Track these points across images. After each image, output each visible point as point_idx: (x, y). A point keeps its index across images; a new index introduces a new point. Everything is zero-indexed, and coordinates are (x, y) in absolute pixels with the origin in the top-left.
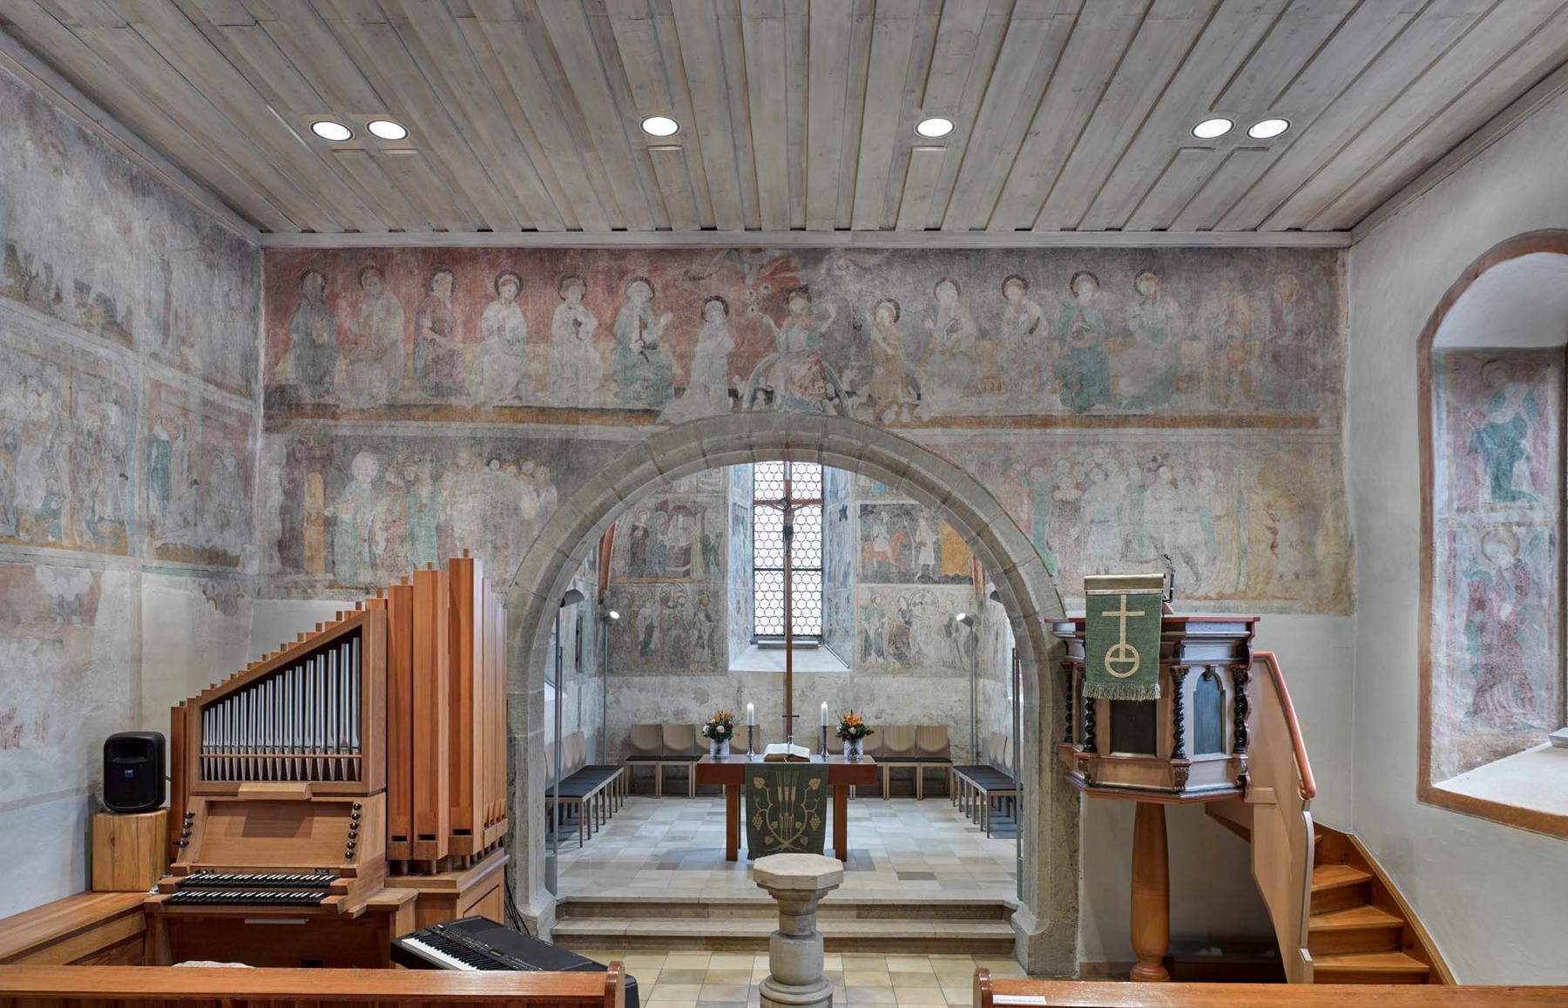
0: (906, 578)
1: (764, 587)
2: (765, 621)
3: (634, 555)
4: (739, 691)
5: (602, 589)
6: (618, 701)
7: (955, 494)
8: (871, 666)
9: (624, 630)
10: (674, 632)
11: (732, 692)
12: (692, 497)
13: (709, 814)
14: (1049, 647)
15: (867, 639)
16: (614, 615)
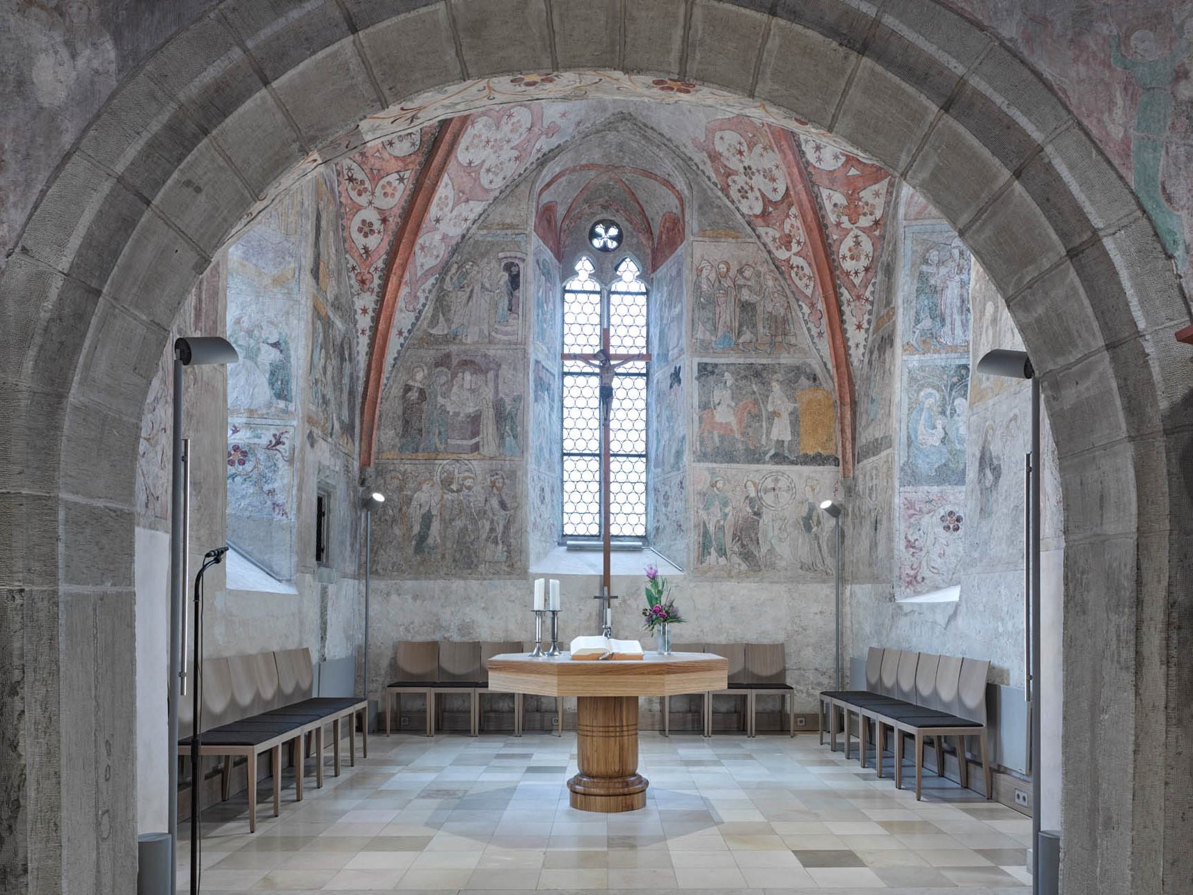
0: (754, 456)
1: (576, 476)
2: (576, 518)
5: (364, 466)
7: (975, 82)
8: (710, 568)
9: (394, 520)
10: (458, 524)
13: (498, 756)
14: (1164, 405)
15: (706, 533)
16: (378, 497)
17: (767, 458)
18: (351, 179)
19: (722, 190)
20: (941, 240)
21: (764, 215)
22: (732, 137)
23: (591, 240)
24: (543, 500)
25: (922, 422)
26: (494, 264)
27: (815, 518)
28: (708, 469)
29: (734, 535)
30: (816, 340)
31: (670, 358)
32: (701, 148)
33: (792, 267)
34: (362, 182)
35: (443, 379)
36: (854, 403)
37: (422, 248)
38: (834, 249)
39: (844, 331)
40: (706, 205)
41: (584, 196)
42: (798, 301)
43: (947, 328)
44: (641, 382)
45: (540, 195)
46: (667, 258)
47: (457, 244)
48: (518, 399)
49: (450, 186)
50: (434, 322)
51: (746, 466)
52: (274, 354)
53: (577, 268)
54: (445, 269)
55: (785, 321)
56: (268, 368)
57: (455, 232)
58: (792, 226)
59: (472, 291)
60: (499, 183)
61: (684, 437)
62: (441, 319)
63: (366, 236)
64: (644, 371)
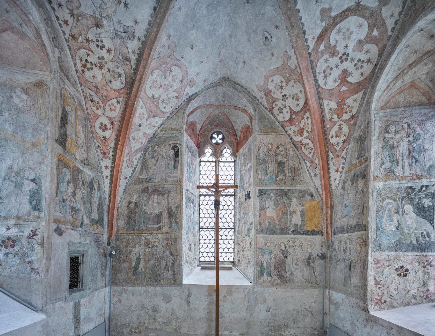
0: (284, 231)
1: (205, 237)
3: (129, 218)
4: (189, 296)
6: (120, 301)
8: (264, 282)
9: (124, 261)
10: (152, 262)
11: (184, 296)
12: (162, 185)
15: (262, 266)
17: (290, 232)
18: (92, 101)
19: (270, 111)
20: (396, 119)
21: (291, 120)
22: (278, 79)
23: (211, 140)
24: (190, 249)
25: (385, 218)
26: (167, 147)
27: (312, 259)
28: (263, 237)
29: (275, 267)
30: (313, 178)
31: (245, 188)
33: (303, 145)
34: (98, 103)
35: (145, 198)
36: (332, 207)
37: (134, 139)
38: (327, 133)
39: (329, 173)
40: (262, 119)
41: (208, 121)
42: (304, 160)
43: (400, 167)
44: (232, 198)
45: (188, 116)
46: (243, 145)
47: (151, 138)
48: (179, 207)
49: (144, 108)
50: (141, 173)
51: (281, 236)
52: (32, 186)
53: (206, 151)
54: (146, 149)
55: (298, 169)
56: (28, 193)
57: (150, 132)
58: (305, 123)
59: (158, 159)
60: (168, 110)
61: (252, 223)
62: (144, 171)
63: (103, 131)
64: (233, 194)
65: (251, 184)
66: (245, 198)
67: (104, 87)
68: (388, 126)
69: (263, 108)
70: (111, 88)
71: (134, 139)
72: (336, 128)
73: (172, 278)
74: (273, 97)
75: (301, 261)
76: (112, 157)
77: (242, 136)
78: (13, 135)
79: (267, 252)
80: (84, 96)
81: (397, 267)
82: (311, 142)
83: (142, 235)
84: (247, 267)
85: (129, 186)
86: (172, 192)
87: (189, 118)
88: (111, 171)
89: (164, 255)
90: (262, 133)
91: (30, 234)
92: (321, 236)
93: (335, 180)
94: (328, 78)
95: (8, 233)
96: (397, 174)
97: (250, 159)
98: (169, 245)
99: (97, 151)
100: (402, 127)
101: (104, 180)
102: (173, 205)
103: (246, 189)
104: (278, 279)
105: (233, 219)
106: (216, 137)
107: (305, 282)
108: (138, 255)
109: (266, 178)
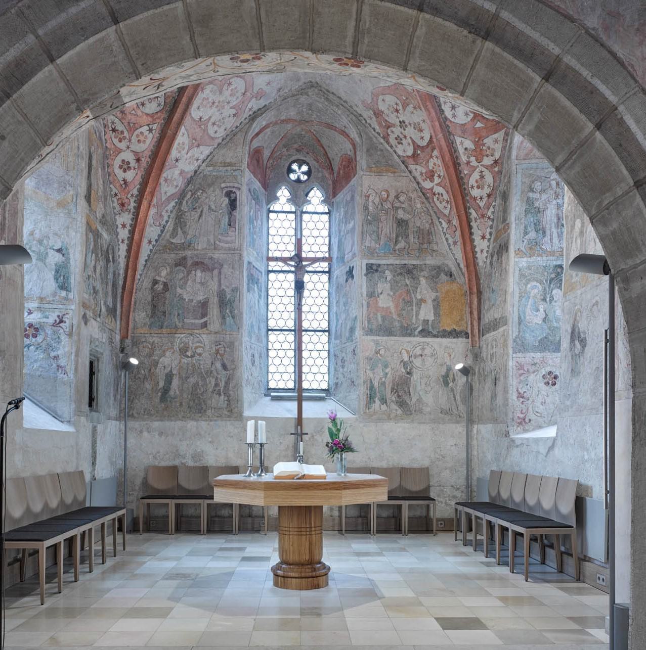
0: (407, 331)
1: (277, 346)
3: (154, 307)
8: (375, 413)
9: (145, 378)
10: (192, 380)
13: (221, 549)
15: (372, 388)
16: (134, 361)
17: (416, 333)
18: (114, 130)
19: (384, 138)
21: (414, 156)
22: (390, 100)
25: (529, 307)
26: (218, 191)
27: (451, 376)
28: (373, 341)
29: (393, 389)
30: (452, 247)
31: (346, 260)
32: (368, 107)
33: (434, 194)
34: (122, 132)
35: (181, 275)
37: (166, 180)
38: (465, 181)
39: (472, 241)
40: (371, 149)
43: (547, 239)
44: (325, 278)
46: (343, 187)
47: (191, 177)
48: (235, 290)
49: (186, 135)
50: (174, 234)
51: (401, 339)
54: (182, 195)
55: (429, 233)
56: (54, 267)
57: (190, 168)
58: (435, 164)
59: (202, 212)
60: (221, 133)
61: (356, 318)
62: (180, 231)
63: (125, 171)
64: (327, 269)
65: (354, 255)
66: (345, 277)
67: (133, 112)
68: (533, 182)
69: (373, 132)
70: (142, 112)
71: (166, 180)
72: (476, 175)
73: (225, 406)
74: (386, 120)
75: (433, 379)
76: (133, 210)
77: (341, 172)
78: (34, 192)
79: (380, 365)
80: (104, 124)
81: (544, 373)
82: (445, 192)
83: (176, 335)
84: (350, 392)
85: (154, 255)
86: (225, 266)
87: (252, 144)
88: (129, 231)
89: (213, 369)
90: (373, 174)
91: (56, 321)
92: (464, 340)
93: (482, 251)
94: (456, 109)
95: (29, 319)
96: (543, 247)
97: (353, 214)
98: (220, 352)
99: (113, 201)
100: (550, 184)
101: (119, 245)
102: (227, 287)
103: (348, 262)
104: (398, 408)
105: (327, 314)
106: (297, 170)
107: (441, 412)
108: (169, 369)
109: (377, 246)
